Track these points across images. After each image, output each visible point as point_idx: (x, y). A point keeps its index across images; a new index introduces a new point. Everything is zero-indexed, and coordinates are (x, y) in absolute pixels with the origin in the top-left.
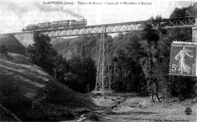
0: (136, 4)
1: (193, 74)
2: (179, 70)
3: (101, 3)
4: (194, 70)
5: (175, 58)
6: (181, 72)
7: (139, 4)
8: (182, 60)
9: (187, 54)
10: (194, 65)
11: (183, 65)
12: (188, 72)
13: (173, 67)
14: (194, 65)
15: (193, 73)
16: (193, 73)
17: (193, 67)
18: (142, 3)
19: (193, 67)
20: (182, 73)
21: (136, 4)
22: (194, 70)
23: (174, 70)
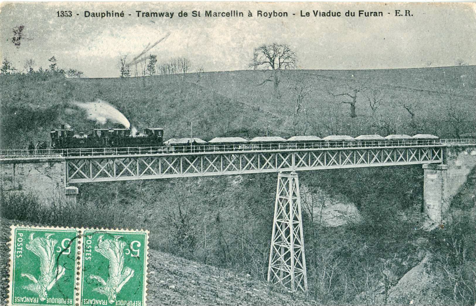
0: (241, 14)
1: (21, 232)
2: (54, 242)
3: (122, 15)
4: (17, 242)
5: (133, 271)
6: (119, 239)
7: (250, 15)
8: (116, 268)
9: (104, 283)
10: (88, 256)
11: (46, 254)
12: (34, 238)
13: (138, 251)
14: (19, 254)
15: (20, 234)
16: (21, 235)
17: (22, 249)
18: (259, 13)
19: (22, 249)
20: (46, 234)
21: (241, 14)
22: (17, 242)
23: (135, 244)
